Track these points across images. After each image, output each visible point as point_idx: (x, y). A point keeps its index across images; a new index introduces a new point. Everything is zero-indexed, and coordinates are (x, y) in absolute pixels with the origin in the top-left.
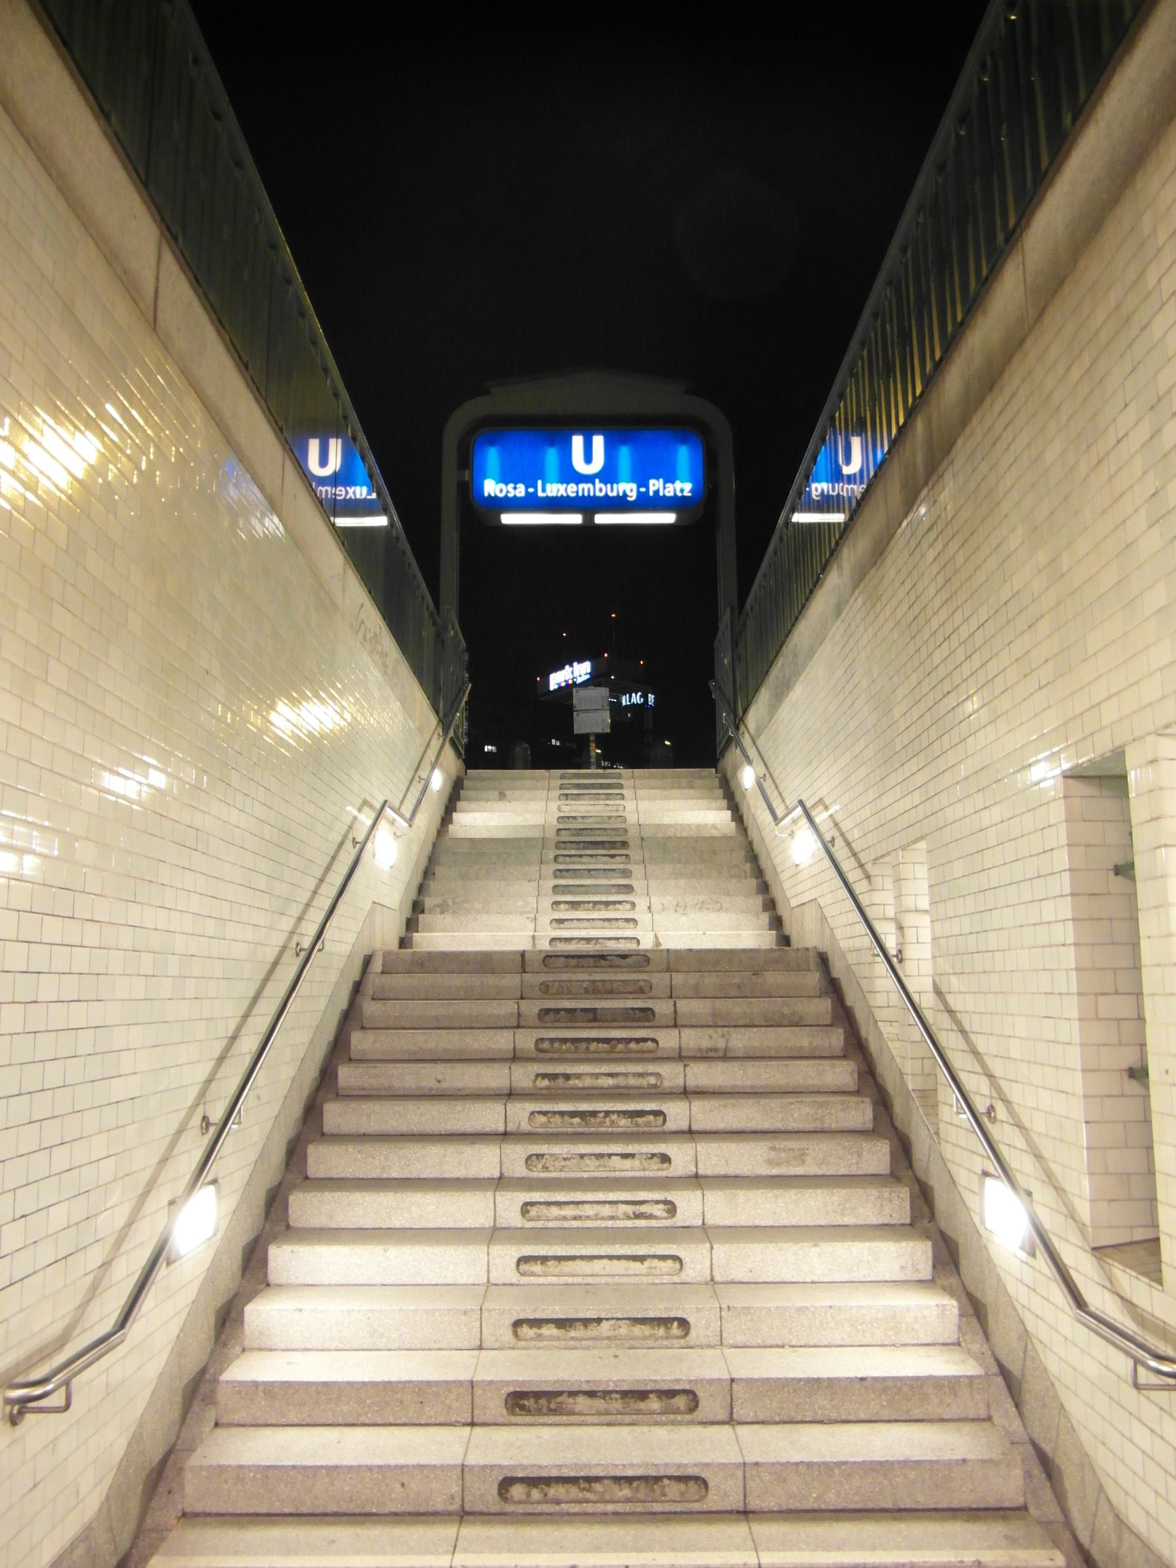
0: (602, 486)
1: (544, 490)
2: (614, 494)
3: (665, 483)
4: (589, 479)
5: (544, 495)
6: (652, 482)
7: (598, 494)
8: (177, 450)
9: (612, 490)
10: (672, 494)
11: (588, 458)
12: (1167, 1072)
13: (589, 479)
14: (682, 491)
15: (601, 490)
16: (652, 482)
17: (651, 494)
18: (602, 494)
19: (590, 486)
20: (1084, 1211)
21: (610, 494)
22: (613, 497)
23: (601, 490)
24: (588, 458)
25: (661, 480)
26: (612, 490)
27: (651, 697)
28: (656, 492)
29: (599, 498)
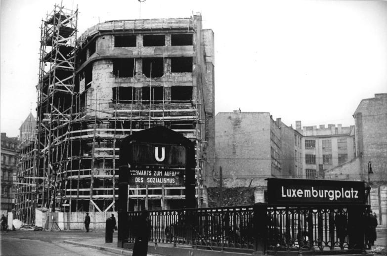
1: (285, 193)
5: (285, 196)
14: (354, 193)
19: (309, 191)
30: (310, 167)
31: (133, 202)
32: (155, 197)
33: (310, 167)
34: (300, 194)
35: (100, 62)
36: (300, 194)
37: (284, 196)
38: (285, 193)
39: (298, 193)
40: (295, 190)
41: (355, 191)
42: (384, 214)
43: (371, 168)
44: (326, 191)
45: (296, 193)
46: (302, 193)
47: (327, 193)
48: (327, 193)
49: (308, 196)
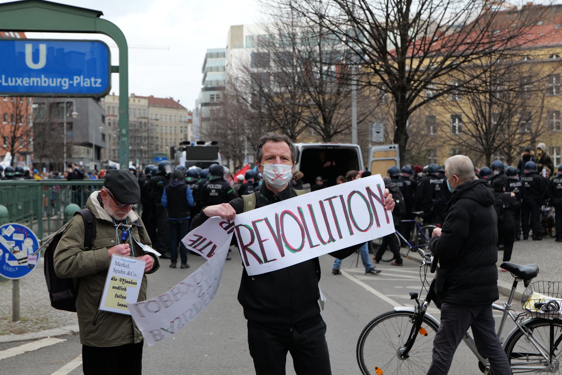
0: (46, 79)
1: (6, 81)
2: (54, 84)
3: (84, 78)
4: (38, 73)
5: (6, 84)
6: (75, 77)
7: (43, 84)
8: (421, 141)
9: (53, 83)
10: (89, 85)
11: (36, 59)
12: (376, 368)
13: (38, 73)
14: (95, 82)
15: (45, 82)
16: (75, 77)
17: (75, 85)
18: (46, 85)
19: (39, 79)
20: (391, 68)
21: (51, 85)
22: (53, 87)
23: (45, 82)
24: (36, 59)
25: (82, 77)
26: (53, 83)
27: (334, 163)
28: (79, 84)
29: (44, 87)
30: (212, 120)
31: (509, 94)
32: (115, 331)
33: (212, 120)
34: (27, 83)
35: (214, 85)
36: (27, 83)
37: (4, 84)
38: (6, 81)
39: (24, 82)
40: (21, 79)
41: (97, 80)
42: (393, 63)
43: (514, 37)
44: (59, 80)
45: (22, 82)
46: (28, 81)
47: (61, 82)
48: (61, 82)
49: (39, 84)
